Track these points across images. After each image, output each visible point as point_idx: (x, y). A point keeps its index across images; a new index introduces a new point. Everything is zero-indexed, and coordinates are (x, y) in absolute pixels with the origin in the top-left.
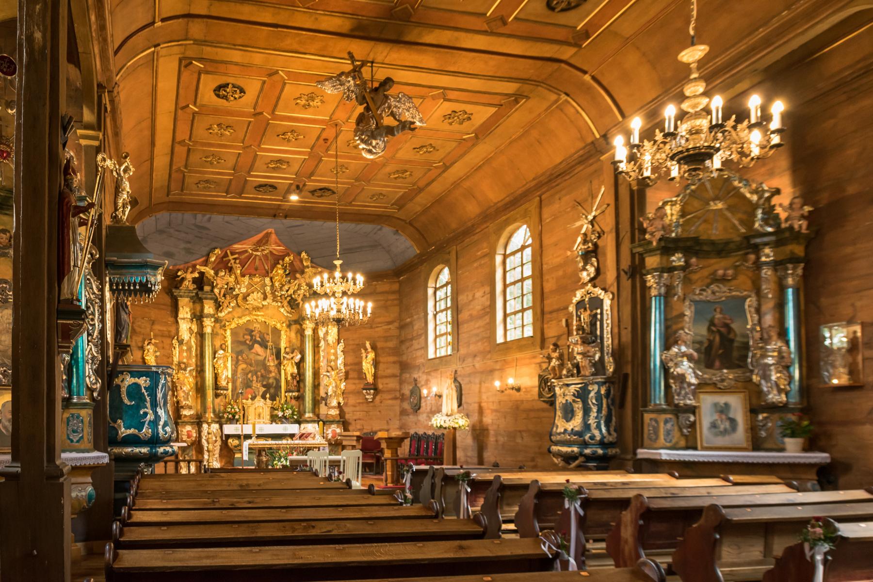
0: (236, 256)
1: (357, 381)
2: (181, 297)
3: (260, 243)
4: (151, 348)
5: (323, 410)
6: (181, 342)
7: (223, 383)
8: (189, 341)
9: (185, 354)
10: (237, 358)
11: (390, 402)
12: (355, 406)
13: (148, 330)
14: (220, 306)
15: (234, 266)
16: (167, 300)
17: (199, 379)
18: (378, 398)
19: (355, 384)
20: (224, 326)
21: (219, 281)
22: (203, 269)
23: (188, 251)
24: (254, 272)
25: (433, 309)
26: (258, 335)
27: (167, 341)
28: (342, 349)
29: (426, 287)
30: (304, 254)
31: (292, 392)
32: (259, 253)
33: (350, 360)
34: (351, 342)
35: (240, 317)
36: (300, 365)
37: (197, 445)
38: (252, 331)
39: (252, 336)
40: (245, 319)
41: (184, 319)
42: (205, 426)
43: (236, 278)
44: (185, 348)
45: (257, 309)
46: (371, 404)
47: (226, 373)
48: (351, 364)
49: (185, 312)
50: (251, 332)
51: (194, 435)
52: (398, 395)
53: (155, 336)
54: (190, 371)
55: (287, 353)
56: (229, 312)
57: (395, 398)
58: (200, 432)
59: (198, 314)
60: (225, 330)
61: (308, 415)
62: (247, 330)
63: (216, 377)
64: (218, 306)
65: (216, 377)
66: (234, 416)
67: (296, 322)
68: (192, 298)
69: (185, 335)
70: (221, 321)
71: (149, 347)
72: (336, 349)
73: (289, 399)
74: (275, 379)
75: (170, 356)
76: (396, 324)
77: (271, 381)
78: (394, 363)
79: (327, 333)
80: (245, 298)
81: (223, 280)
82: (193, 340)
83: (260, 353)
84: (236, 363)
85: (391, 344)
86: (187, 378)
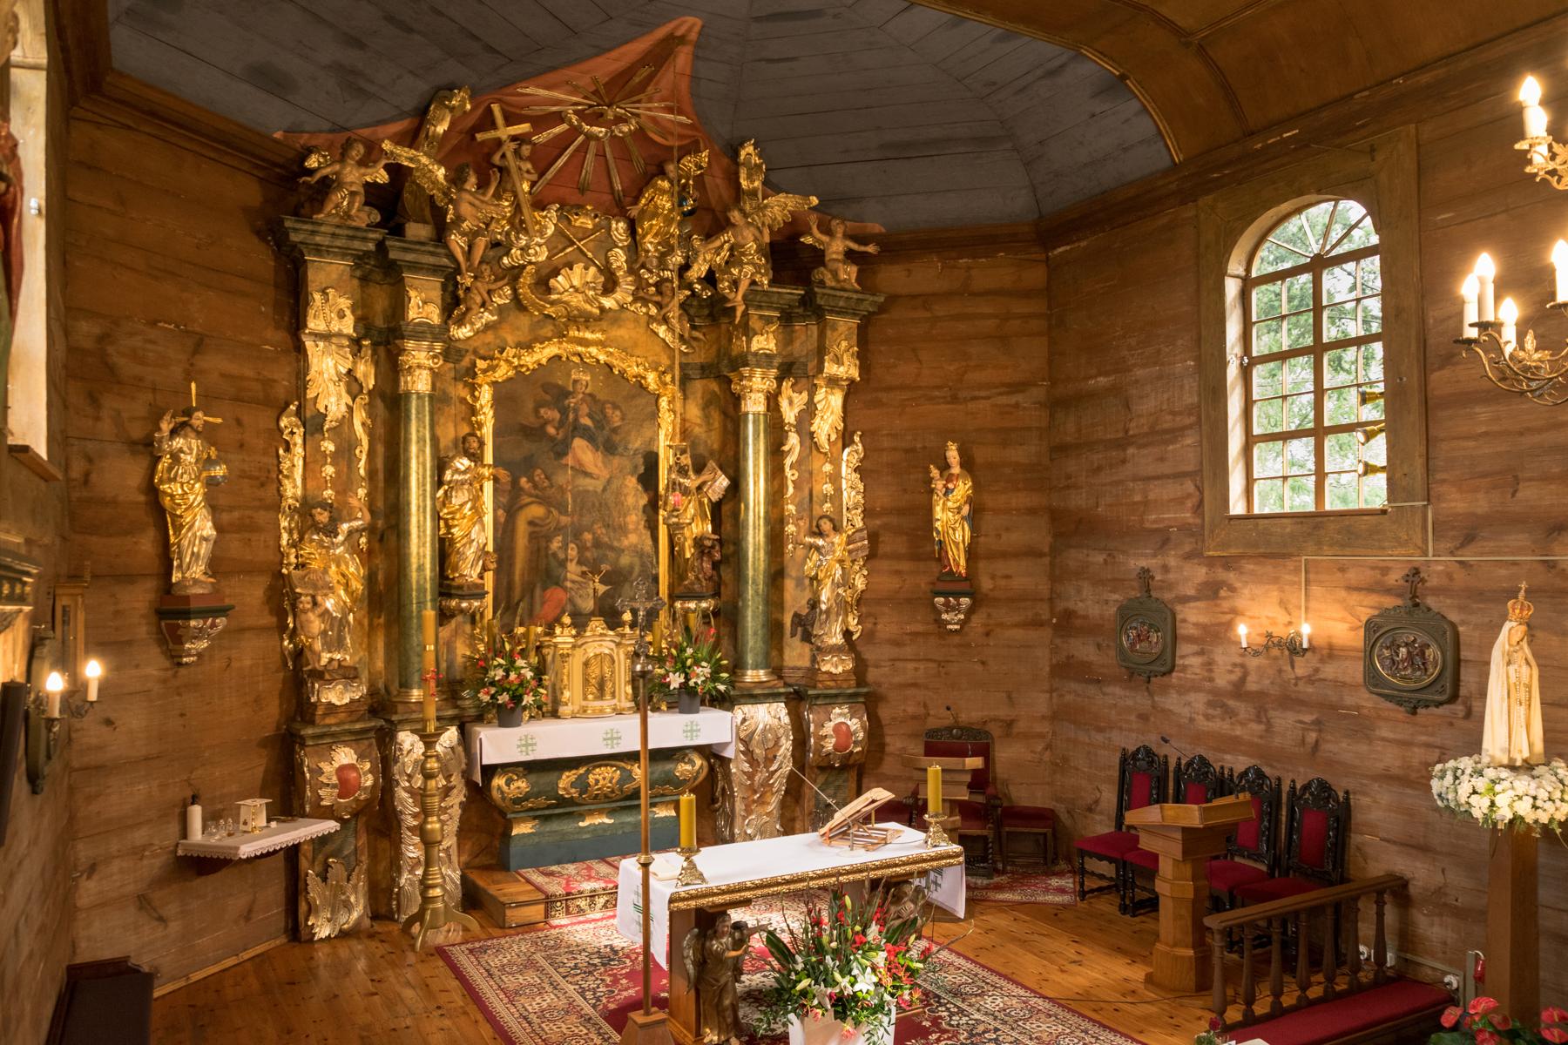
0: (524, 128)
1: (905, 566)
2: (318, 250)
3: (622, 86)
4: (189, 447)
5: (796, 654)
6: (314, 424)
7: (469, 570)
8: (347, 420)
9: (329, 470)
10: (515, 483)
11: (1018, 634)
12: (897, 643)
13: (177, 371)
14: (457, 302)
15: (511, 162)
16: (262, 260)
17: (379, 561)
18: (977, 620)
19: (898, 572)
20: (471, 371)
21: (465, 209)
22: (404, 155)
23: (352, 82)
24: (575, 198)
25: (1238, 350)
26: (585, 409)
27: (257, 419)
28: (855, 461)
29: (1222, 274)
30: (747, 151)
31: (700, 598)
32: (599, 131)
33: (884, 498)
34: (886, 443)
35: (528, 347)
36: (726, 511)
37: (378, 818)
38: (567, 394)
39: (564, 412)
40: (544, 353)
41: (326, 337)
42: (407, 740)
43: (517, 208)
44: (329, 446)
45: (585, 320)
46: (956, 639)
47: (477, 535)
48: (885, 512)
49: (331, 313)
50: (559, 395)
51: (368, 781)
52: (1044, 612)
53: (209, 400)
54: (350, 533)
55: (683, 471)
56: (488, 327)
57: (1037, 624)
58: (386, 763)
59: (380, 322)
60: (473, 388)
61: (754, 675)
62: (547, 387)
63: (444, 551)
64: (453, 304)
65: (444, 551)
66: (517, 699)
67: (706, 370)
68: (360, 259)
69: (332, 400)
70: (460, 354)
71: (179, 442)
72: (836, 463)
73: (694, 622)
74: (641, 555)
75: (272, 477)
76: (1038, 393)
77: (625, 560)
78: (1032, 511)
79: (810, 411)
80: (543, 285)
81: (473, 210)
82: (359, 417)
83: (591, 469)
84: (509, 506)
85: (1019, 454)
86: (338, 561)
